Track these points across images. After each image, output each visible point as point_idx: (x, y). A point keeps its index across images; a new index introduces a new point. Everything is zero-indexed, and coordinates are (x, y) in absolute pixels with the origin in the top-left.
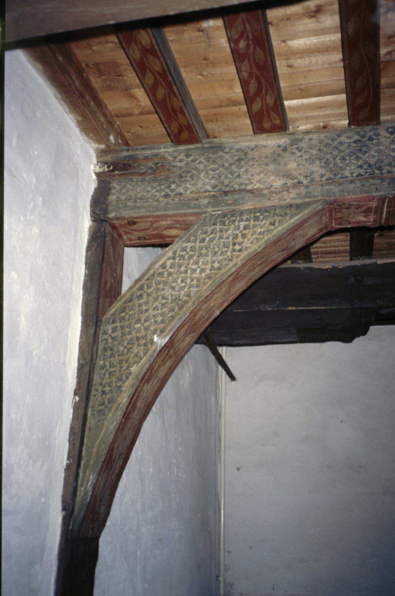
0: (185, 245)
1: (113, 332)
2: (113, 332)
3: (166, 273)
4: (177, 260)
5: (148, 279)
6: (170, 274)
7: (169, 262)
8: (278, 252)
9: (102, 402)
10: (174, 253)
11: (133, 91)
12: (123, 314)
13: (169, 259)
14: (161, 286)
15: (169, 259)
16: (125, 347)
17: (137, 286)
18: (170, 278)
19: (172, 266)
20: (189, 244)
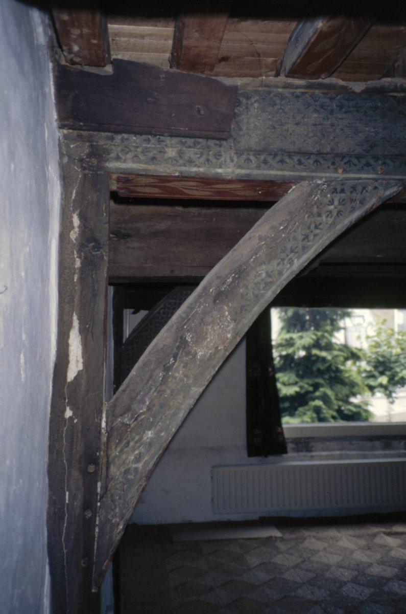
0: (170, 301)
1: (132, 350)
2: (132, 350)
3: (160, 318)
4: (166, 309)
5: (150, 320)
6: (163, 318)
7: (162, 311)
8: (62, 50)
9: (247, 161)
10: (165, 305)
11: (296, 357)
12: (137, 340)
13: (161, 309)
14: (158, 325)
15: (161, 309)
16: (281, 105)
17: (144, 324)
18: (163, 321)
19: (164, 313)
20: (174, 301)
